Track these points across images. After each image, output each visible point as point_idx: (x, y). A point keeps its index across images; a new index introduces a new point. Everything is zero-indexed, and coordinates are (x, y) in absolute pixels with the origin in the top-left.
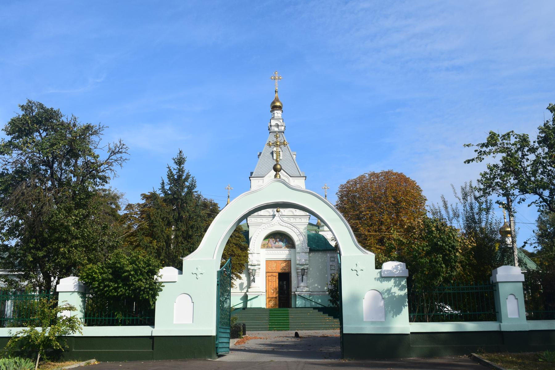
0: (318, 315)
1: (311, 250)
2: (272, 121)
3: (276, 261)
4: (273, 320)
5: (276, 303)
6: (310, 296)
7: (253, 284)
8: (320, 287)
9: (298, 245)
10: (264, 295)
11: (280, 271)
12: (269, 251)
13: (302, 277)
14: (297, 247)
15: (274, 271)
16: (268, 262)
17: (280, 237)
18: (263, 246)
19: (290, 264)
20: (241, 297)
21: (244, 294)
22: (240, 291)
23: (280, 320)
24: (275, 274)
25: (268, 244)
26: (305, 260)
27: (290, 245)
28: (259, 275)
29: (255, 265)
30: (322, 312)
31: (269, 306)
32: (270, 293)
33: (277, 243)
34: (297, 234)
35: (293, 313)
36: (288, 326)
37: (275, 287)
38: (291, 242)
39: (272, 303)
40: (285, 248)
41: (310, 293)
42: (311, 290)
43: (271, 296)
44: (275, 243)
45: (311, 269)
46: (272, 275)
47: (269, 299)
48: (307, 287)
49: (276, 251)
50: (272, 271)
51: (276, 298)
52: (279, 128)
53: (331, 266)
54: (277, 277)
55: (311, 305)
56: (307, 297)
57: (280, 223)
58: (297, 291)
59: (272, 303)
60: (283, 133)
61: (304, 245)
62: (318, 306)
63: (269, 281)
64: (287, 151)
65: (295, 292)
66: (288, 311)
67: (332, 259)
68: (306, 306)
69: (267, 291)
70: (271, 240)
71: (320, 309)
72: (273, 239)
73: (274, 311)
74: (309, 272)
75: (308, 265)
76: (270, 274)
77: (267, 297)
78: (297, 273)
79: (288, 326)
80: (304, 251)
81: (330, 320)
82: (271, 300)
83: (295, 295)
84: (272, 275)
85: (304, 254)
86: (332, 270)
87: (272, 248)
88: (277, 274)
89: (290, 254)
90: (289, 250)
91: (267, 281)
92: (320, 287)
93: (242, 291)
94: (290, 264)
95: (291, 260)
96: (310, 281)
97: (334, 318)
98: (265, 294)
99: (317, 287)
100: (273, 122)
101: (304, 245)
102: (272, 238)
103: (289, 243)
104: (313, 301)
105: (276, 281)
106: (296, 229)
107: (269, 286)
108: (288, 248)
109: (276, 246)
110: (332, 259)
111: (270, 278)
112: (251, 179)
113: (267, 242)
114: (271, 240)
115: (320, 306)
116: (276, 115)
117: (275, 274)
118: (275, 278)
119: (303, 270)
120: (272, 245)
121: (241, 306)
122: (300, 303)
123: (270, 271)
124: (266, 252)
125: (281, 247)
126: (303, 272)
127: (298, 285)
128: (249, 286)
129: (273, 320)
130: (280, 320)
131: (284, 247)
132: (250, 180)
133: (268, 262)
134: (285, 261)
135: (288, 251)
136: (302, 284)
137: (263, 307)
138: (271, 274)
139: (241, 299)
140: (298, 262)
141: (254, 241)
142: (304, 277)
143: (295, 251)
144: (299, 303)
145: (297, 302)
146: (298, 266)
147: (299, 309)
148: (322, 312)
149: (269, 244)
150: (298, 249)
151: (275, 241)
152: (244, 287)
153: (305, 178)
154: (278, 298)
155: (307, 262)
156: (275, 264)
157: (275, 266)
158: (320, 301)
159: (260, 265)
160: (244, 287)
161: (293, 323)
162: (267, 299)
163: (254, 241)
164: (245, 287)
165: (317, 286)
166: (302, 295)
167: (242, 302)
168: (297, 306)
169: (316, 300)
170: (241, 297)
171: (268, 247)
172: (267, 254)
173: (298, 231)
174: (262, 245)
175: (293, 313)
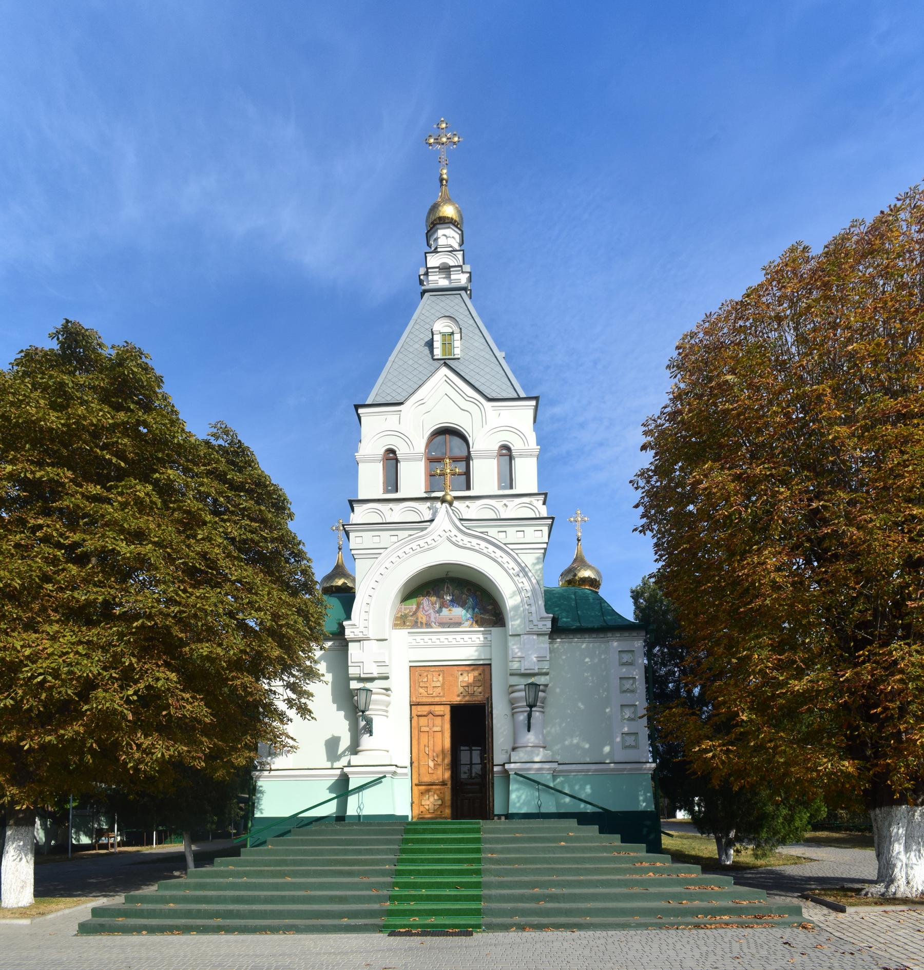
0: (605, 849)
1: (558, 630)
2: (429, 257)
3: (445, 669)
4: (410, 873)
5: (442, 799)
6: (554, 777)
7: (366, 741)
8: (587, 746)
9: (516, 608)
10: (406, 774)
11: (457, 700)
12: (418, 638)
13: (529, 716)
14: (510, 614)
15: (437, 699)
16: (417, 671)
17: (457, 592)
18: (401, 621)
19: (488, 677)
20: (331, 782)
21: (338, 772)
22: (329, 765)
23: (440, 873)
24: (442, 708)
25: (415, 613)
26: (541, 659)
27: (486, 617)
28: (387, 711)
29: (371, 680)
30: (618, 836)
31: (422, 809)
32: (423, 770)
33: (445, 611)
34: (511, 572)
35: (498, 840)
36: (473, 906)
37: (439, 748)
38: (490, 607)
39: (432, 799)
40: (471, 626)
41: (555, 765)
42: (558, 758)
43: (427, 779)
44: (439, 611)
45: (558, 690)
46: (430, 713)
47: (422, 787)
48: (544, 747)
49: (442, 637)
50: (430, 700)
51: (443, 783)
52: (453, 277)
53: (624, 682)
54: (448, 717)
55: (558, 804)
56: (547, 779)
57: (454, 539)
58: (510, 763)
59: (430, 802)
60: (463, 293)
61: (533, 609)
62: (583, 808)
63: (420, 731)
64: (476, 337)
65: (503, 765)
66: (478, 831)
67: (626, 658)
68: (543, 810)
69: (415, 764)
70: (425, 602)
71: (583, 819)
72: (434, 599)
73: (424, 831)
74: (550, 700)
75: (546, 674)
76: (425, 709)
77: (415, 781)
78: (512, 702)
79: (473, 906)
80: (535, 629)
81: (656, 871)
82: (428, 791)
83: (506, 774)
84: (430, 713)
85: (535, 637)
86: (625, 692)
87: (428, 625)
88: (447, 710)
89: (487, 645)
90: (483, 633)
91: (415, 733)
92: (587, 746)
93: (336, 765)
94: (488, 677)
95: (490, 665)
96: (554, 730)
97: (601, 832)
98: (408, 771)
99: (577, 746)
100: (434, 261)
101: (533, 609)
102: (428, 594)
103: (484, 610)
104: (566, 791)
105: (442, 731)
106: (506, 558)
107: (422, 747)
108: (481, 625)
109: (444, 621)
110: (626, 658)
111: (423, 721)
112: (360, 411)
113: (414, 607)
114: (428, 603)
115: (589, 809)
116: (442, 241)
117: (438, 709)
118: (438, 721)
119: (533, 689)
120: (429, 616)
121: (330, 809)
122: (523, 797)
123: (425, 700)
124: (410, 639)
125: (459, 624)
126: (532, 695)
127: (515, 741)
128: (354, 749)
129: (410, 873)
130: (440, 873)
131: (469, 623)
132: (358, 415)
133: (417, 671)
134: (474, 667)
135: (481, 637)
136: (531, 738)
137: (400, 812)
138: (426, 709)
139: (331, 789)
140: (515, 665)
141: (367, 600)
142: (536, 714)
143: (505, 633)
144: (519, 798)
145: (513, 796)
146: (514, 680)
147: (526, 824)
148: (618, 836)
149: (420, 614)
150: (514, 623)
151: (437, 606)
152: (340, 752)
153: (533, 403)
154: (449, 783)
155: (546, 666)
156: (441, 678)
157: (438, 684)
158: (588, 789)
159: (387, 678)
160: (340, 752)
161: (501, 885)
162: (415, 788)
163: (367, 600)
164: (344, 752)
165: (578, 744)
166: (531, 774)
167: (334, 795)
168: (512, 810)
169: (577, 787)
170: (332, 782)
171: (415, 624)
172: (412, 647)
173: (512, 564)
174: (396, 618)
175: (498, 840)
